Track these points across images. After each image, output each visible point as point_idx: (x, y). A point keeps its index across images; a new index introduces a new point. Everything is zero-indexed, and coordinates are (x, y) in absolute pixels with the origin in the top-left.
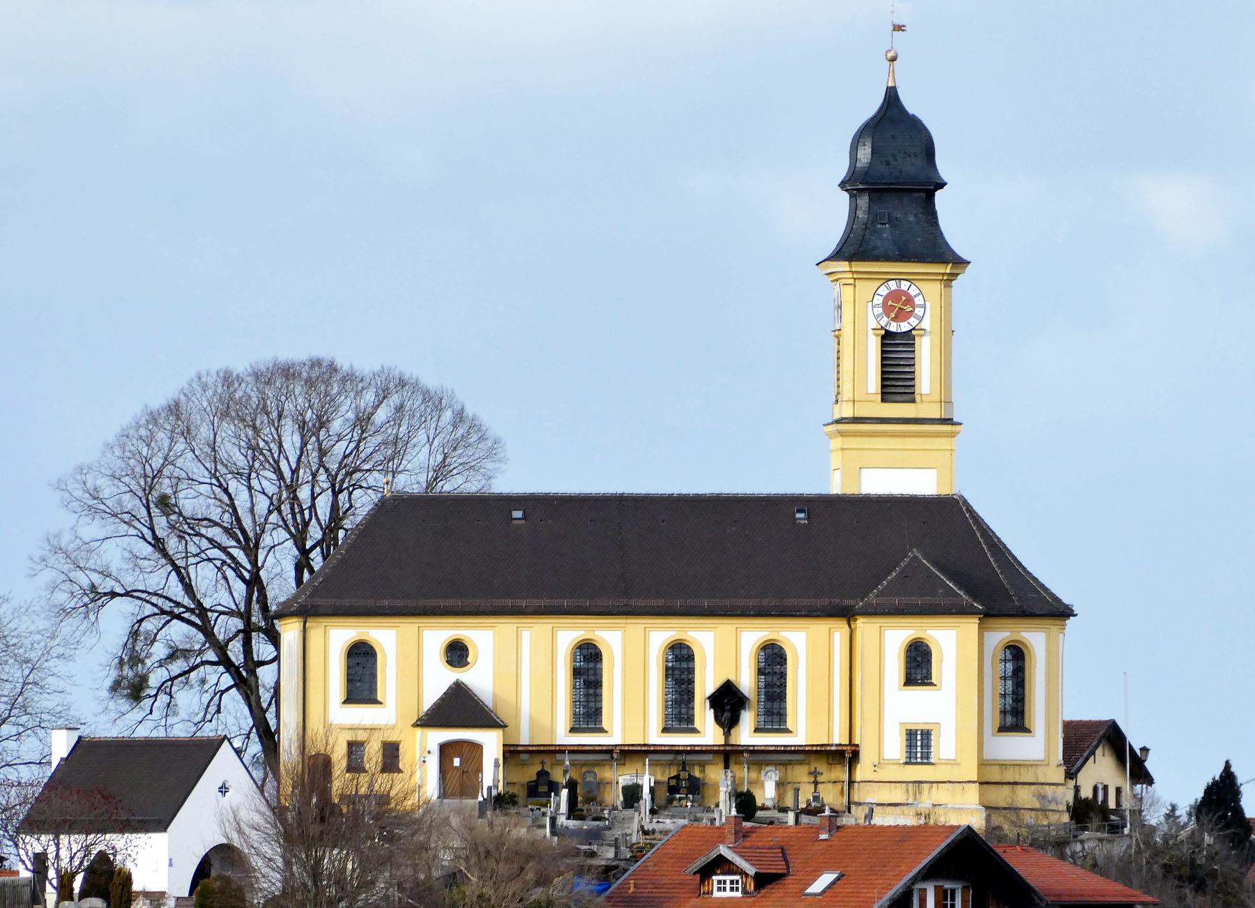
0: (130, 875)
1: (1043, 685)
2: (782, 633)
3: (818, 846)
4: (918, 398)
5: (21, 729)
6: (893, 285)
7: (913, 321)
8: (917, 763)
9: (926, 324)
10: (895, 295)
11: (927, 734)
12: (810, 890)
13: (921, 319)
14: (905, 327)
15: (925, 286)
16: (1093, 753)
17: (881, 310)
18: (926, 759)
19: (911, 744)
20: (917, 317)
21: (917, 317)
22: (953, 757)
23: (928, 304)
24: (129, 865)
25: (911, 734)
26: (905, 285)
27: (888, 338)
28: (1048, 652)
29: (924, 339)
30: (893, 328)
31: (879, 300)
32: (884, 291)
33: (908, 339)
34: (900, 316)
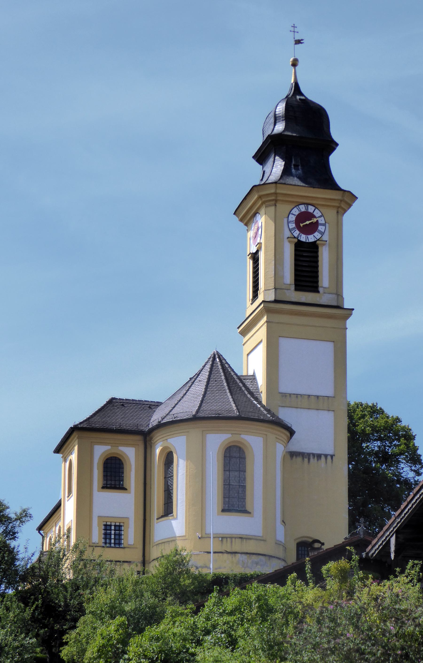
2: (243, 436)
4: (321, 290)
6: (303, 208)
7: (317, 235)
8: (111, 547)
9: (326, 237)
11: (119, 528)
12: (393, 559)
13: (322, 234)
14: (311, 239)
15: (325, 211)
16: (326, 549)
17: (294, 225)
18: (118, 543)
19: (107, 536)
22: (261, 535)
23: (327, 225)
25: (107, 527)
26: (311, 209)
27: (299, 247)
28: (266, 457)
29: (324, 247)
30: (303, 238)
31: (292, 218)
32: (296, 212)
33: (314, 247)
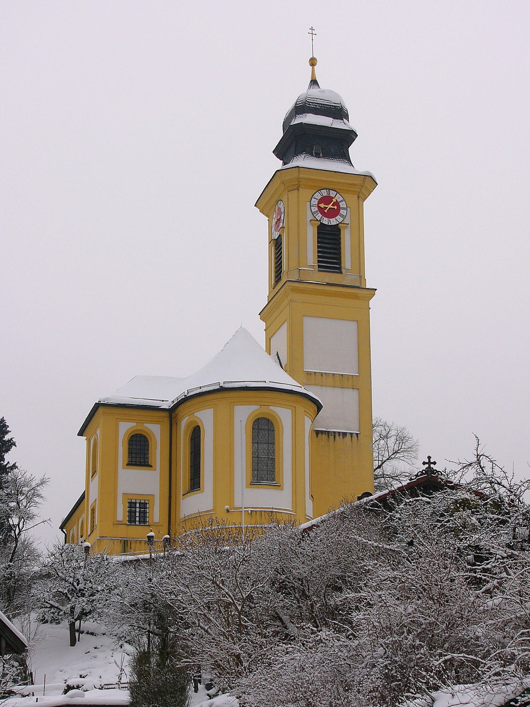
0: (265, 314)
1: (306, 496)
3: (4, 506)
4: (343, 270)
5: (496, 486)
6: (325, 193)
7: (339, 219)
10: (326, 200)
11: (144, 505)
13: (344, 217)
14: (333, 222)
20: (342, 216)
21: (342, 216)
24: (258, 329)
25: (132, 505)
27: (322, 229)
30: (325, 221)
31: (315, 202)
32: (318, 196)
34: (333, 213)
